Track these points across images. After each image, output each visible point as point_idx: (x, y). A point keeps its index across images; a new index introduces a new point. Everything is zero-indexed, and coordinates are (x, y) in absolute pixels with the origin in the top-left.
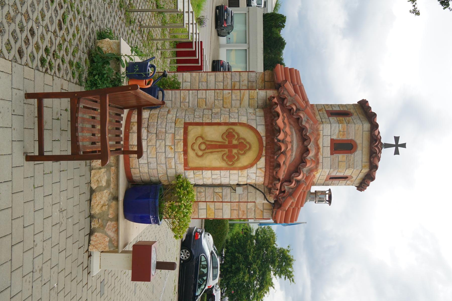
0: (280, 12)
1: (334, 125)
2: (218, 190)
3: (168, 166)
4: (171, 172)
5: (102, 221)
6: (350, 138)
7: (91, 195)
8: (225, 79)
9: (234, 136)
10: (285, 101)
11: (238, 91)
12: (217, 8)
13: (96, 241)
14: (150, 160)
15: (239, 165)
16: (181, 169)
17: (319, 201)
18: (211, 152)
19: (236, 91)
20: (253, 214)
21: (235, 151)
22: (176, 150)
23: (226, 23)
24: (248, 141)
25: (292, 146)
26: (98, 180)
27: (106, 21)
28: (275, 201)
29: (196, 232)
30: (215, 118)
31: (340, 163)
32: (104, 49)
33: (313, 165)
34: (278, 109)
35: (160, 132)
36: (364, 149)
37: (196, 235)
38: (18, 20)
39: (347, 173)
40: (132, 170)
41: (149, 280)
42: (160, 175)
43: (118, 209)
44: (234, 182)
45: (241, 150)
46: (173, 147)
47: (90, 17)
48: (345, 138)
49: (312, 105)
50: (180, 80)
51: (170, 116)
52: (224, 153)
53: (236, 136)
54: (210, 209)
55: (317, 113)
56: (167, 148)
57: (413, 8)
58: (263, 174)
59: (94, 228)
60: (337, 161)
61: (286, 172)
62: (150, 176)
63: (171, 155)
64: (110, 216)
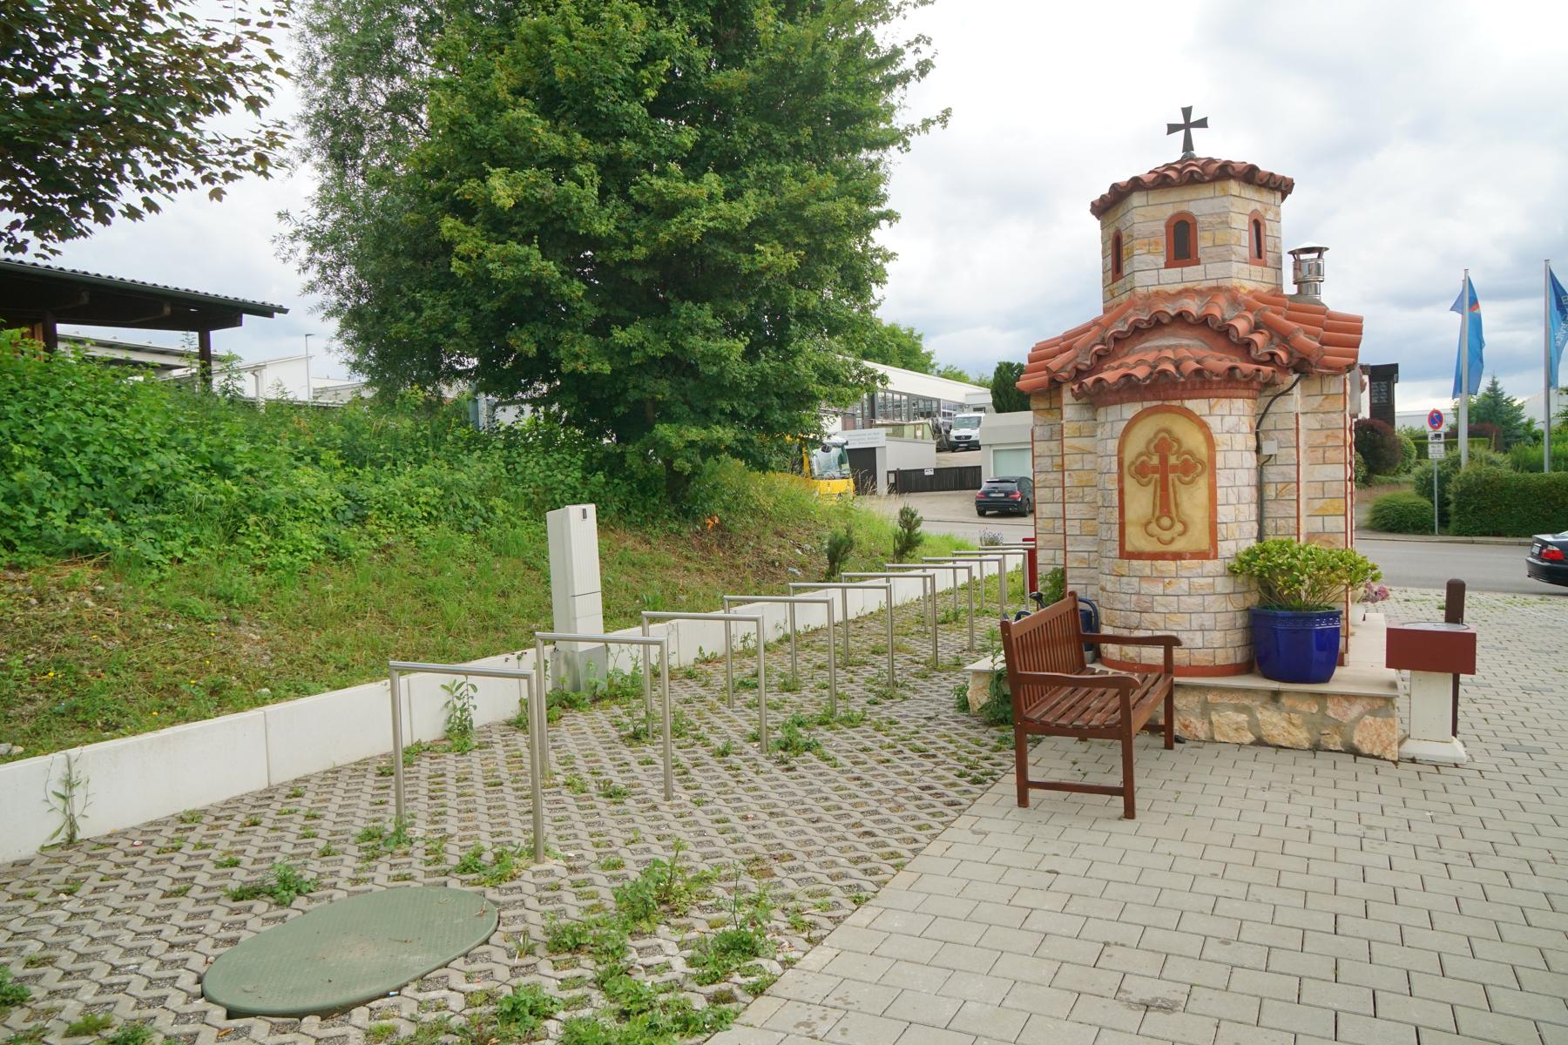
0: (990, 375)
1: (1136, 265)
2: (1270, 492)
3: (1208, 591)
4: (1223, 585)
5: (1325, 727)
6: (1163, 229)
7: (1267, 745)
8: (1047, 484)
9: (1143, 462)
10: (1082, 367)
11: (1066, 458)
12: (982, 513)
13: (1374, 744)
14: (1195, 626)
15: (1202, 451)
16: (1211, 566)
17: (1318, 273)
18: (1177, 505)
19: (1066, 462)
20: (1334, 415)
21: (1173, 460)
22: (1174, 574)
23: (1014, 493)
24: (1151, 435)
25: (1168, 347)
26: (1236, 730)
27: (943, 699)
28: (1295, 372)
29: (1540, 556)
30: (1111, 501)
31: (1217, 242)
32: (984, 700)
33: (1222, 301)
34: (1089, 381)
35: (1137, 604)
36: (1187, 197)
37: (1550, 556)
38: (902, 801)
39: (1241, 223)
40: (1220, 661)
41: (1474, 635)
42: (1230, 608)
43: (1298, 693)
44: (1251, 460)
45: (1170, 448)
46: (1167, 580)
47: (930, 719)
48: (1163, 239)
49: (1106, 310)
50: (1051, 568)
51: (1109, 587)
52: (1177, 482)
53: (1144, 458)
54: (1321, 508)
55: (1117, 300)
56: (1168, 592)
57: (938, 124)
58: (1225, 402)
59: (1343, 744)
60: (1214, 249)
61: (1223, 355)
62: (1234, 627)
63: (1184, 585)
64: (1315, 709)
